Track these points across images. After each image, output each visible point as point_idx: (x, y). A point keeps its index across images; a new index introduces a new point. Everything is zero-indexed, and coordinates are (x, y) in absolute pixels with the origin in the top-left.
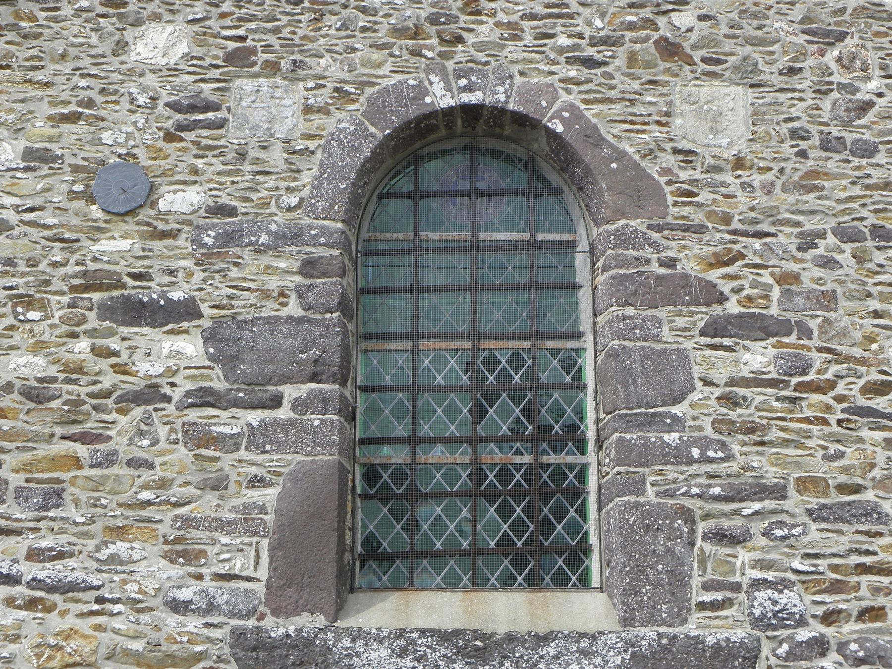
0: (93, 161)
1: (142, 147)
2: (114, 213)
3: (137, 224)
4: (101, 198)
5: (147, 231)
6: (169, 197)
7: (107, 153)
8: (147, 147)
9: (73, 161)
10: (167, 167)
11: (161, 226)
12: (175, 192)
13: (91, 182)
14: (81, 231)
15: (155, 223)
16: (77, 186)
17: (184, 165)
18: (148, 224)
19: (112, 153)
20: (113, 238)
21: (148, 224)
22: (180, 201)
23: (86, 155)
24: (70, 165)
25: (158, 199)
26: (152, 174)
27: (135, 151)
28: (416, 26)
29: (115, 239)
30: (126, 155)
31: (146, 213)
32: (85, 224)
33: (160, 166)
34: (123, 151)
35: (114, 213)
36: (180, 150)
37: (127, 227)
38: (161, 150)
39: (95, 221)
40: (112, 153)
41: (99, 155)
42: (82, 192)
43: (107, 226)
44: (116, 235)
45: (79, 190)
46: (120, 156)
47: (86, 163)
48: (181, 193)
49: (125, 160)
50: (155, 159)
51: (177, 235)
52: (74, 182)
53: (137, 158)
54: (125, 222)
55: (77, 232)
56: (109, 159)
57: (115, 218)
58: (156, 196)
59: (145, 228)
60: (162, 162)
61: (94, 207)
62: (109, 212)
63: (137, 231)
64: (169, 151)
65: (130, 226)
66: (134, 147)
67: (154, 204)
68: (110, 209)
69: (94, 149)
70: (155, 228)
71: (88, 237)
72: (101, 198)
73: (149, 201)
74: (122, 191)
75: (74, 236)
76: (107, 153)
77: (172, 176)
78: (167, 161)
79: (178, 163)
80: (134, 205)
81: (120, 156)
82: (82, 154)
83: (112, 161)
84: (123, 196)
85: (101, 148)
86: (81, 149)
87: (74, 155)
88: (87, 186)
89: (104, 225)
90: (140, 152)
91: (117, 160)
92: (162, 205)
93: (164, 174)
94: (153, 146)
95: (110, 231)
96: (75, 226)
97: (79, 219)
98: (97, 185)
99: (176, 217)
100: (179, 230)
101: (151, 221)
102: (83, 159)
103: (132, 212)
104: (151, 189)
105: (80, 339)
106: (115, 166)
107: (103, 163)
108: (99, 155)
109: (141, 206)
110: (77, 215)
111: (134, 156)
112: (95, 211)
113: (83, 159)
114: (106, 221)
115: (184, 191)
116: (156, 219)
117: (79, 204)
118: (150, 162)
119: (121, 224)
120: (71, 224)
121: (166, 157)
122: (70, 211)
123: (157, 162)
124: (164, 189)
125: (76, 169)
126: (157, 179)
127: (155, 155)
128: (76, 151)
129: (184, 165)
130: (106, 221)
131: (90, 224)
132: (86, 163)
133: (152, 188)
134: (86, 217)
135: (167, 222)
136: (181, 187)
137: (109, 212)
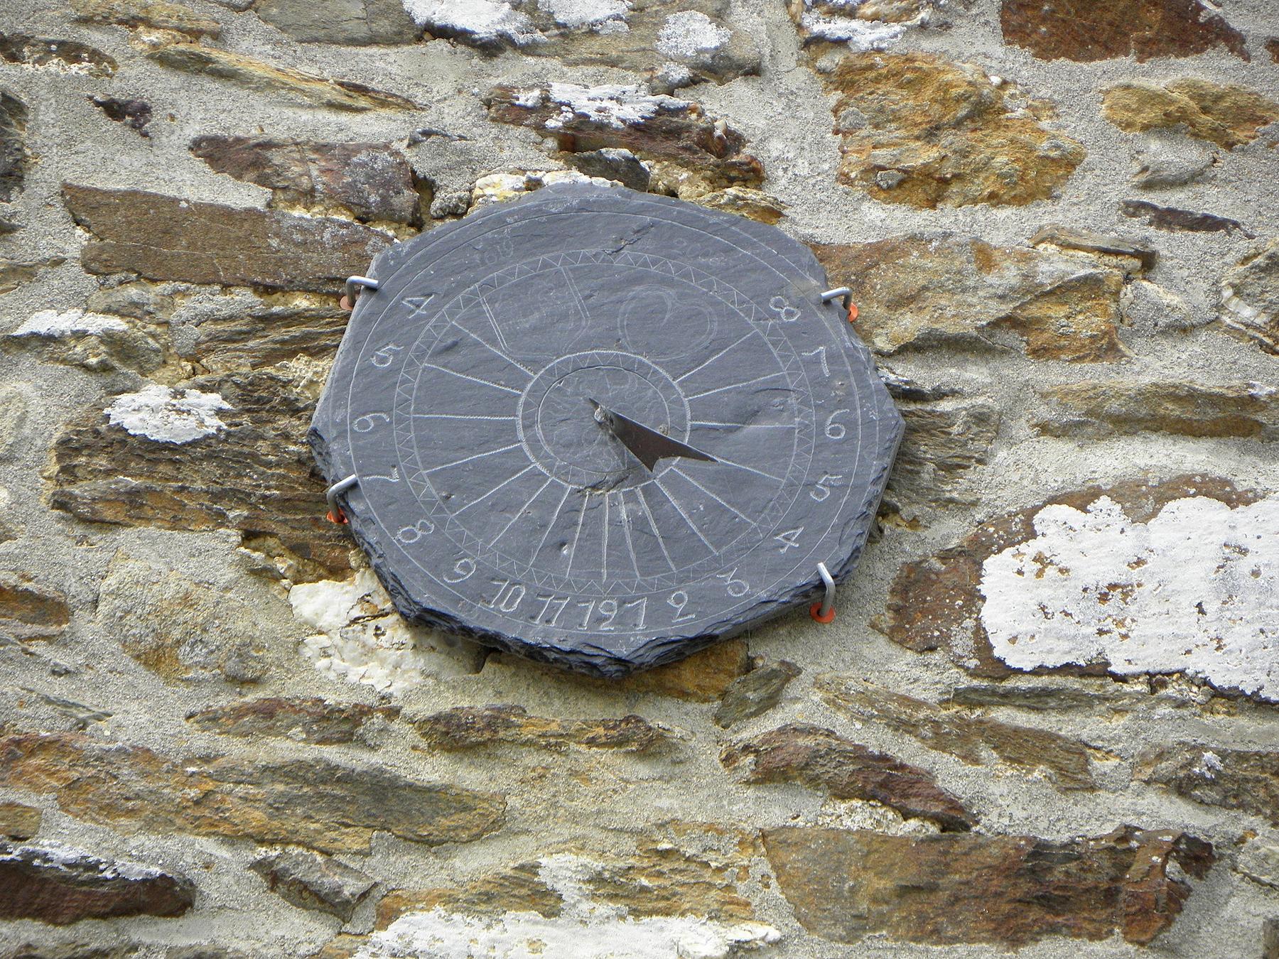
0: (315, 174)
1: (795, 76)
2: (537, 662)
3: (774, 771)
4: (404, 507)
5: (872, 843)
6: (1090, 544)
7: (455, 114)
8: (846, 80)
9: (116, 166)
10: (1055, 265)
11: (1012, 804)
12: (1142, 498)
13: (300, 368)
14: (203, 814)
15: (952, 774)
16: (154, 393)
17: (1226, 258)
18: (885, 782)
19: (504, 109)
20: (529, 892)
21: (885, 782)
22: (1195, 580)
23: (245, 117)
24: (81, 204)
25: (974, 553)
26: (909, 324)
27: (725, 107)
28: (589, 881)
29: (545, 901)
30: (641, 132)
31: (850, 682)
32: (235, 749)
33: (984, 257)
34: (620, 101)
35: (537, 662)
36: (1172, 124)
37: (668, 801)
38: (983, 111)
39: (345, 724)
40: (504, 109)
41: (371, 126)
42: (202, 449)
43: (471, 777)
44: (561, 868)
45: (181, 430)
46: (579, 142)
47: (244, 195)
48: (1195, 519)
49: (634, 177)
50: (928, 187)
51: (1176, 898)
52: (123, 360)
53: (753, 175)
54: (652, 747)
55: (161, 818)
56: (471, 164)
57: (547, 710)
58: (952, 531)
59: (857, 816)
60: (1005, 226)
61: (326, 602)
62: (485, 649)
63: (766, 839)
64: (1070, 130)
65: (697, 787)
66: (715, 69)
67: (931, 601)
68: (501, 615)
69: (326, 66)
70: (954, 820)
71: (274, 877)
72: (404, 507)
73: (882, 573)
74: (609, 457)
75: (137, 854)
76: (455, 114)
77: (1106, 348)
78: (1044, 215)
79: (1161, 241)
80: (743, 590)
81: (579, 142)
82: (200, 111)
83: (499, 186)
84: (622, 507)
85: (388, 66)
86: (199, 66)
87: (128, 113)
88: (258, 400)
89: (434, 770)
90: (780, 123)
91: (558, 175)
92: (1016, 610)
93: (1016, 329)
94: (910, 76)
95: (493, 824)
96: (142, 756)
97: (178, 700)
98: (368, 389)
99: (1165, 726)
100: (1197, 855)
101: (909, 751)
102: (217, 152)
103: (705, 661)
104: (903, 463)
105: (587, 931)
106: (538, 224)
107: (409, 199)
108: (371, 126)
109: (809, 608)
110: (156, 658)
111: (726, 158)
112: (340, 636)
113: (217, 152)
114: (449, 735)
115: (1229, 495)
116: (961, 739)
117: (173, 566)
118: (883, 219)
119: (611, 767)
120: (102, 737)
121: (1040, 178)
122: (88, 626)
123: (950, 218)
124: (1022, 466)
125: (136, 239)
126: (945, 373)
127: (924, 155)
128: (135, 78)
129: (1226, 258)
130: (449, 735)
131: (290, 747)
132: (244, 195)
133: (917, 453)
134: (249, 690)
135: (1072, 769)
136: (1193, 457)
137: (485, 649)
